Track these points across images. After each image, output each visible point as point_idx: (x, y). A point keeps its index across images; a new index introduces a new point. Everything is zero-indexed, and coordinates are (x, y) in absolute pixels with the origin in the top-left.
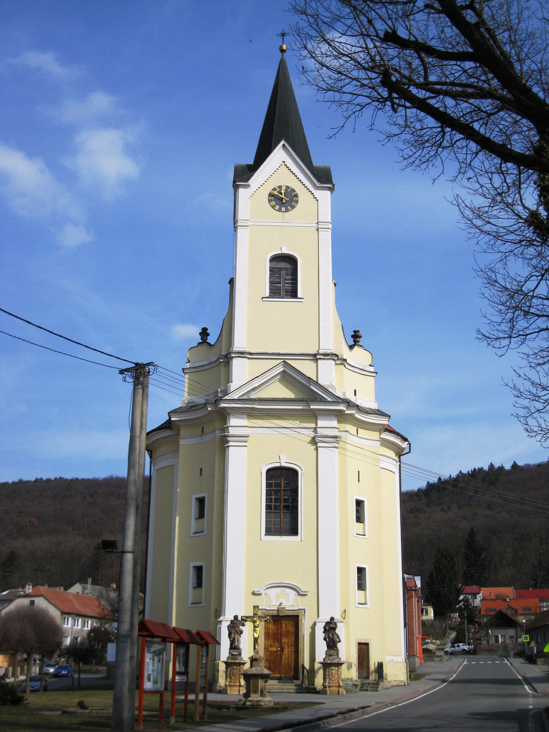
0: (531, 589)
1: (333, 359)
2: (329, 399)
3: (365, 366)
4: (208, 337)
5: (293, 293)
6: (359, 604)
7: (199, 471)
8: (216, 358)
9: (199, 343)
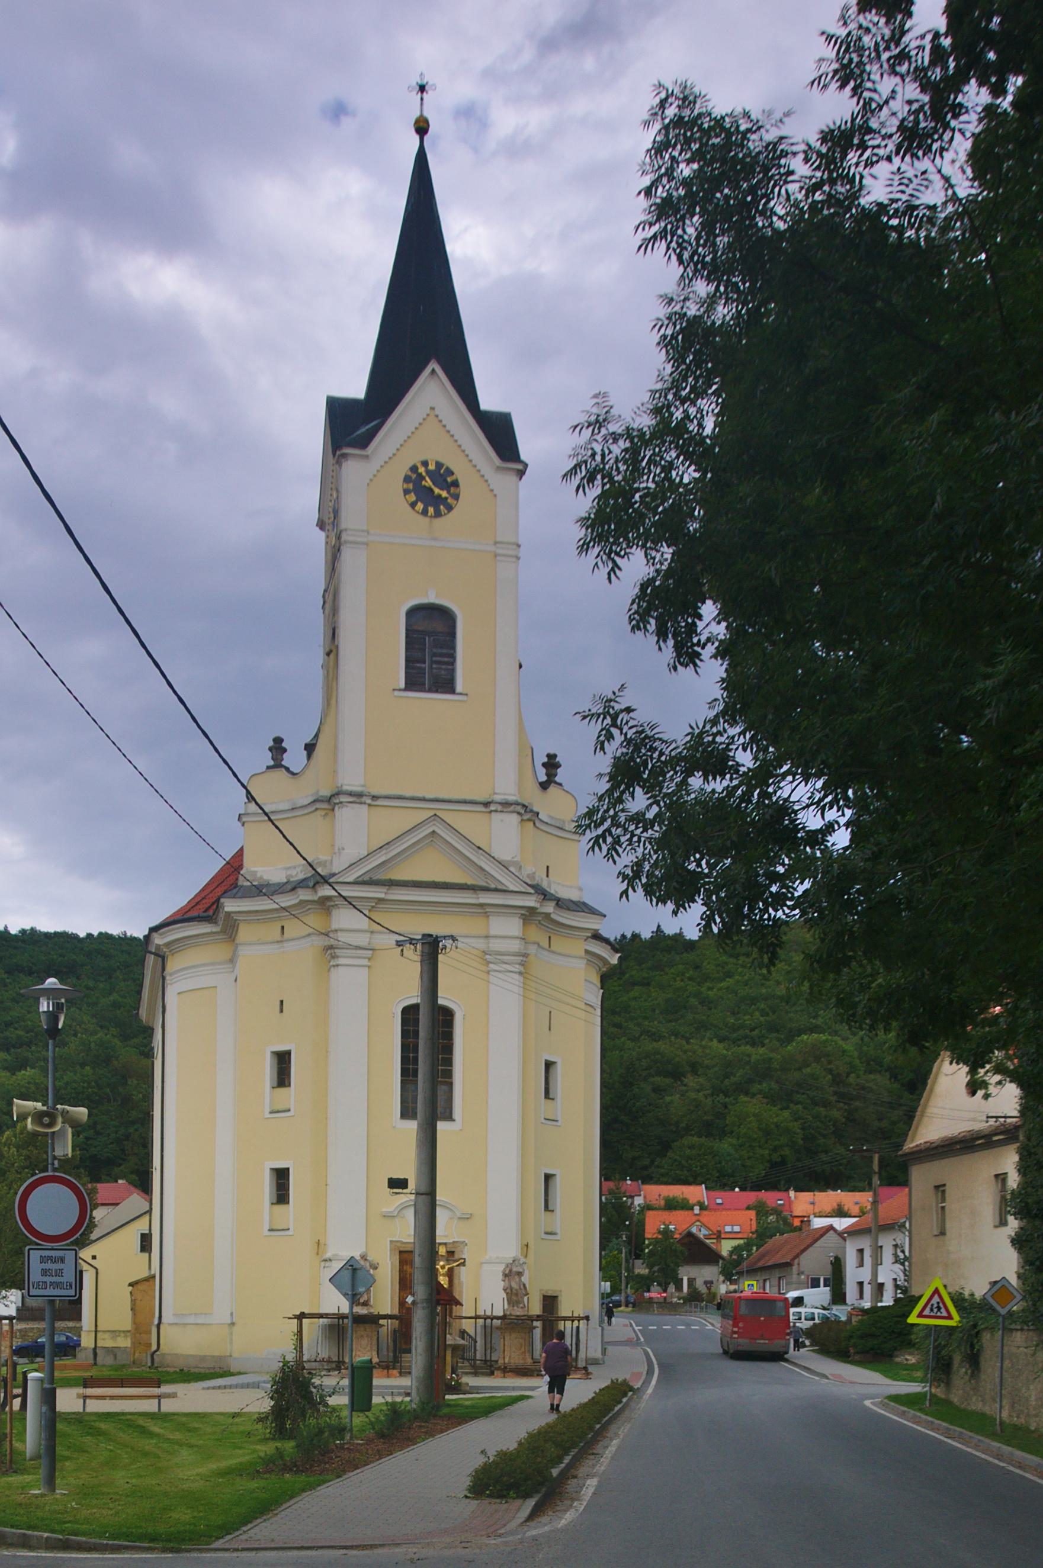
0: (737, 1189)
1: (519, 813)
2: (512, 888)
3: (564, 822)
4: (285, 756)
5: (445, 684)
6: (546, 1233)
7: (278, 1003)
8: (310, 800)
9: (268, 768)
